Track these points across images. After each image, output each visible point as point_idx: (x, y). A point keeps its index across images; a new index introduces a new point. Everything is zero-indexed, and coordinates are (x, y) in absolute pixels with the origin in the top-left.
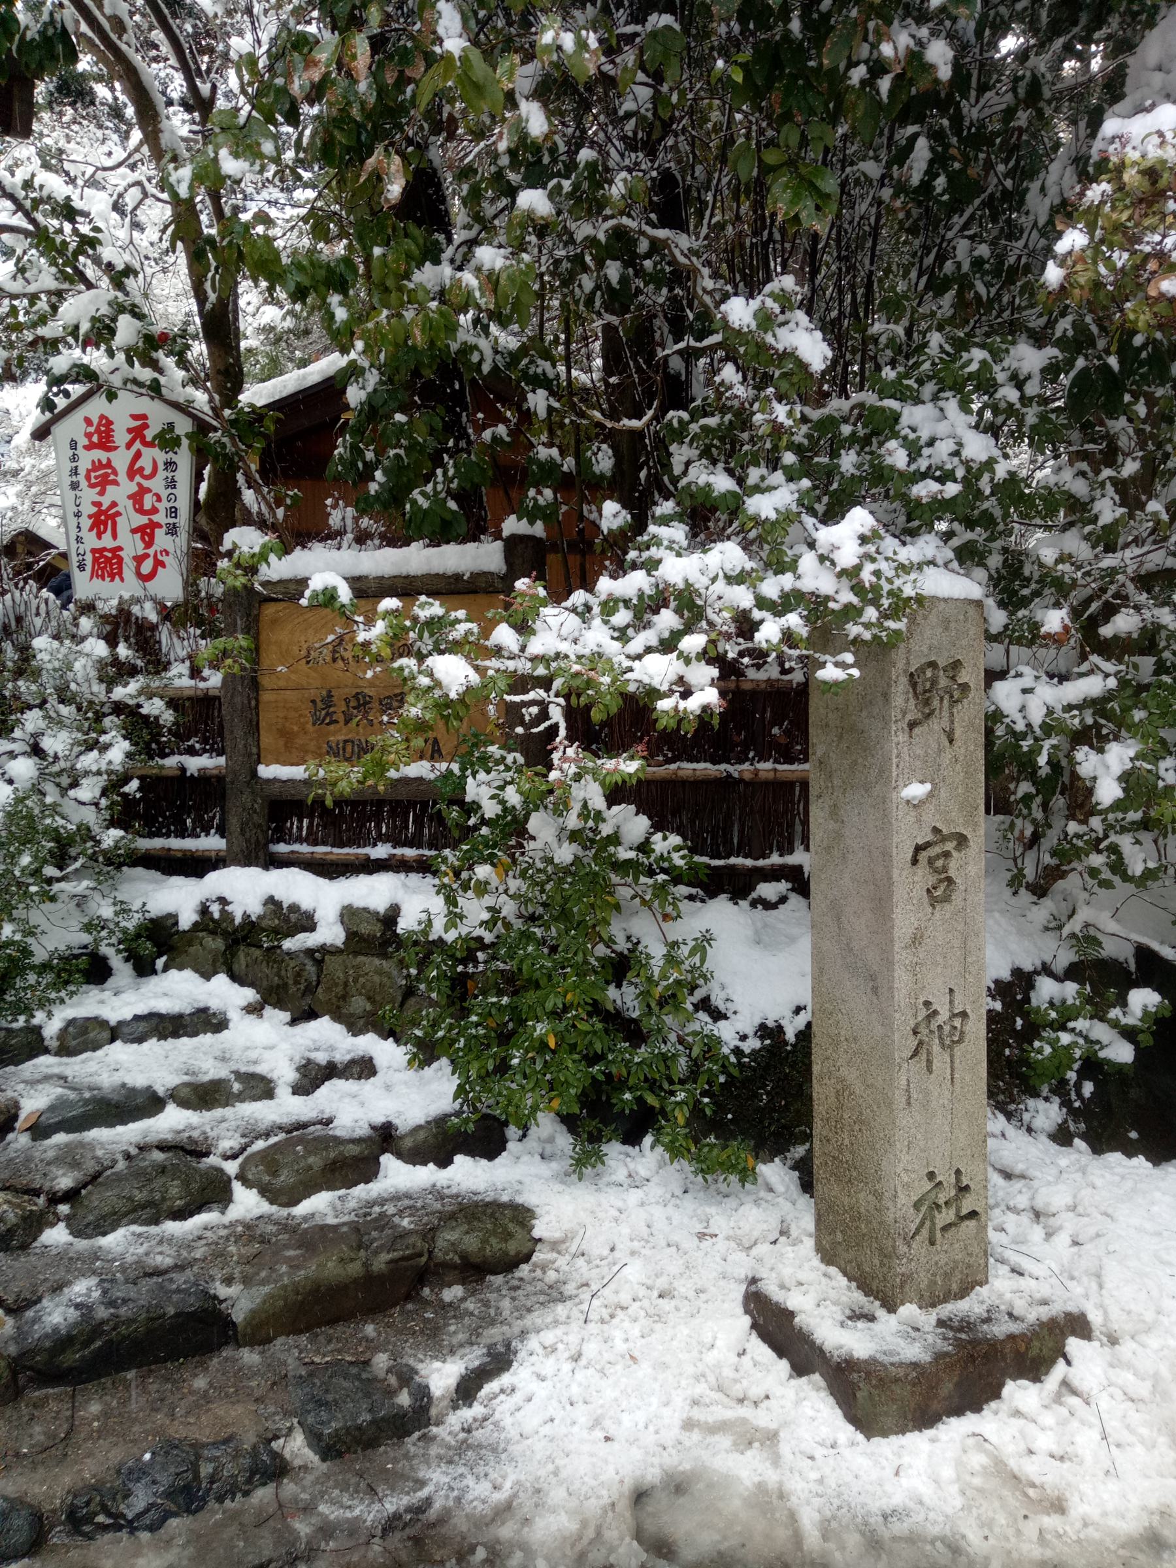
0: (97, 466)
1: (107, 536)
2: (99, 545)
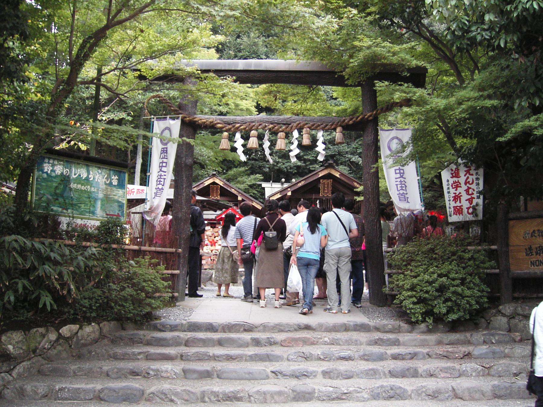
0: (454, 182)
2: (456, 205)
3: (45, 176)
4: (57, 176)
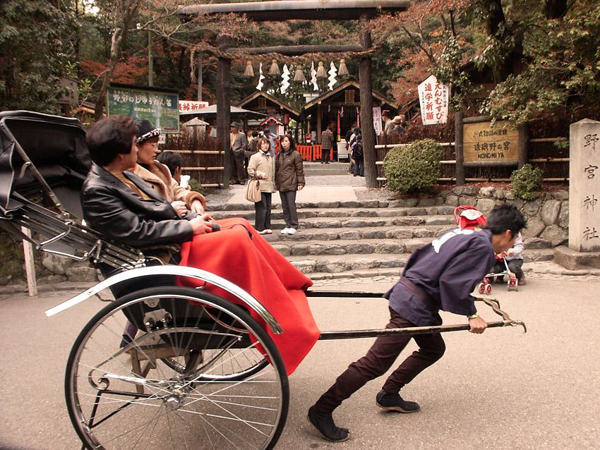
1: (430, 110)
3: (115, 103)
4: (124, 104)
